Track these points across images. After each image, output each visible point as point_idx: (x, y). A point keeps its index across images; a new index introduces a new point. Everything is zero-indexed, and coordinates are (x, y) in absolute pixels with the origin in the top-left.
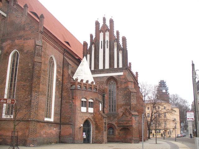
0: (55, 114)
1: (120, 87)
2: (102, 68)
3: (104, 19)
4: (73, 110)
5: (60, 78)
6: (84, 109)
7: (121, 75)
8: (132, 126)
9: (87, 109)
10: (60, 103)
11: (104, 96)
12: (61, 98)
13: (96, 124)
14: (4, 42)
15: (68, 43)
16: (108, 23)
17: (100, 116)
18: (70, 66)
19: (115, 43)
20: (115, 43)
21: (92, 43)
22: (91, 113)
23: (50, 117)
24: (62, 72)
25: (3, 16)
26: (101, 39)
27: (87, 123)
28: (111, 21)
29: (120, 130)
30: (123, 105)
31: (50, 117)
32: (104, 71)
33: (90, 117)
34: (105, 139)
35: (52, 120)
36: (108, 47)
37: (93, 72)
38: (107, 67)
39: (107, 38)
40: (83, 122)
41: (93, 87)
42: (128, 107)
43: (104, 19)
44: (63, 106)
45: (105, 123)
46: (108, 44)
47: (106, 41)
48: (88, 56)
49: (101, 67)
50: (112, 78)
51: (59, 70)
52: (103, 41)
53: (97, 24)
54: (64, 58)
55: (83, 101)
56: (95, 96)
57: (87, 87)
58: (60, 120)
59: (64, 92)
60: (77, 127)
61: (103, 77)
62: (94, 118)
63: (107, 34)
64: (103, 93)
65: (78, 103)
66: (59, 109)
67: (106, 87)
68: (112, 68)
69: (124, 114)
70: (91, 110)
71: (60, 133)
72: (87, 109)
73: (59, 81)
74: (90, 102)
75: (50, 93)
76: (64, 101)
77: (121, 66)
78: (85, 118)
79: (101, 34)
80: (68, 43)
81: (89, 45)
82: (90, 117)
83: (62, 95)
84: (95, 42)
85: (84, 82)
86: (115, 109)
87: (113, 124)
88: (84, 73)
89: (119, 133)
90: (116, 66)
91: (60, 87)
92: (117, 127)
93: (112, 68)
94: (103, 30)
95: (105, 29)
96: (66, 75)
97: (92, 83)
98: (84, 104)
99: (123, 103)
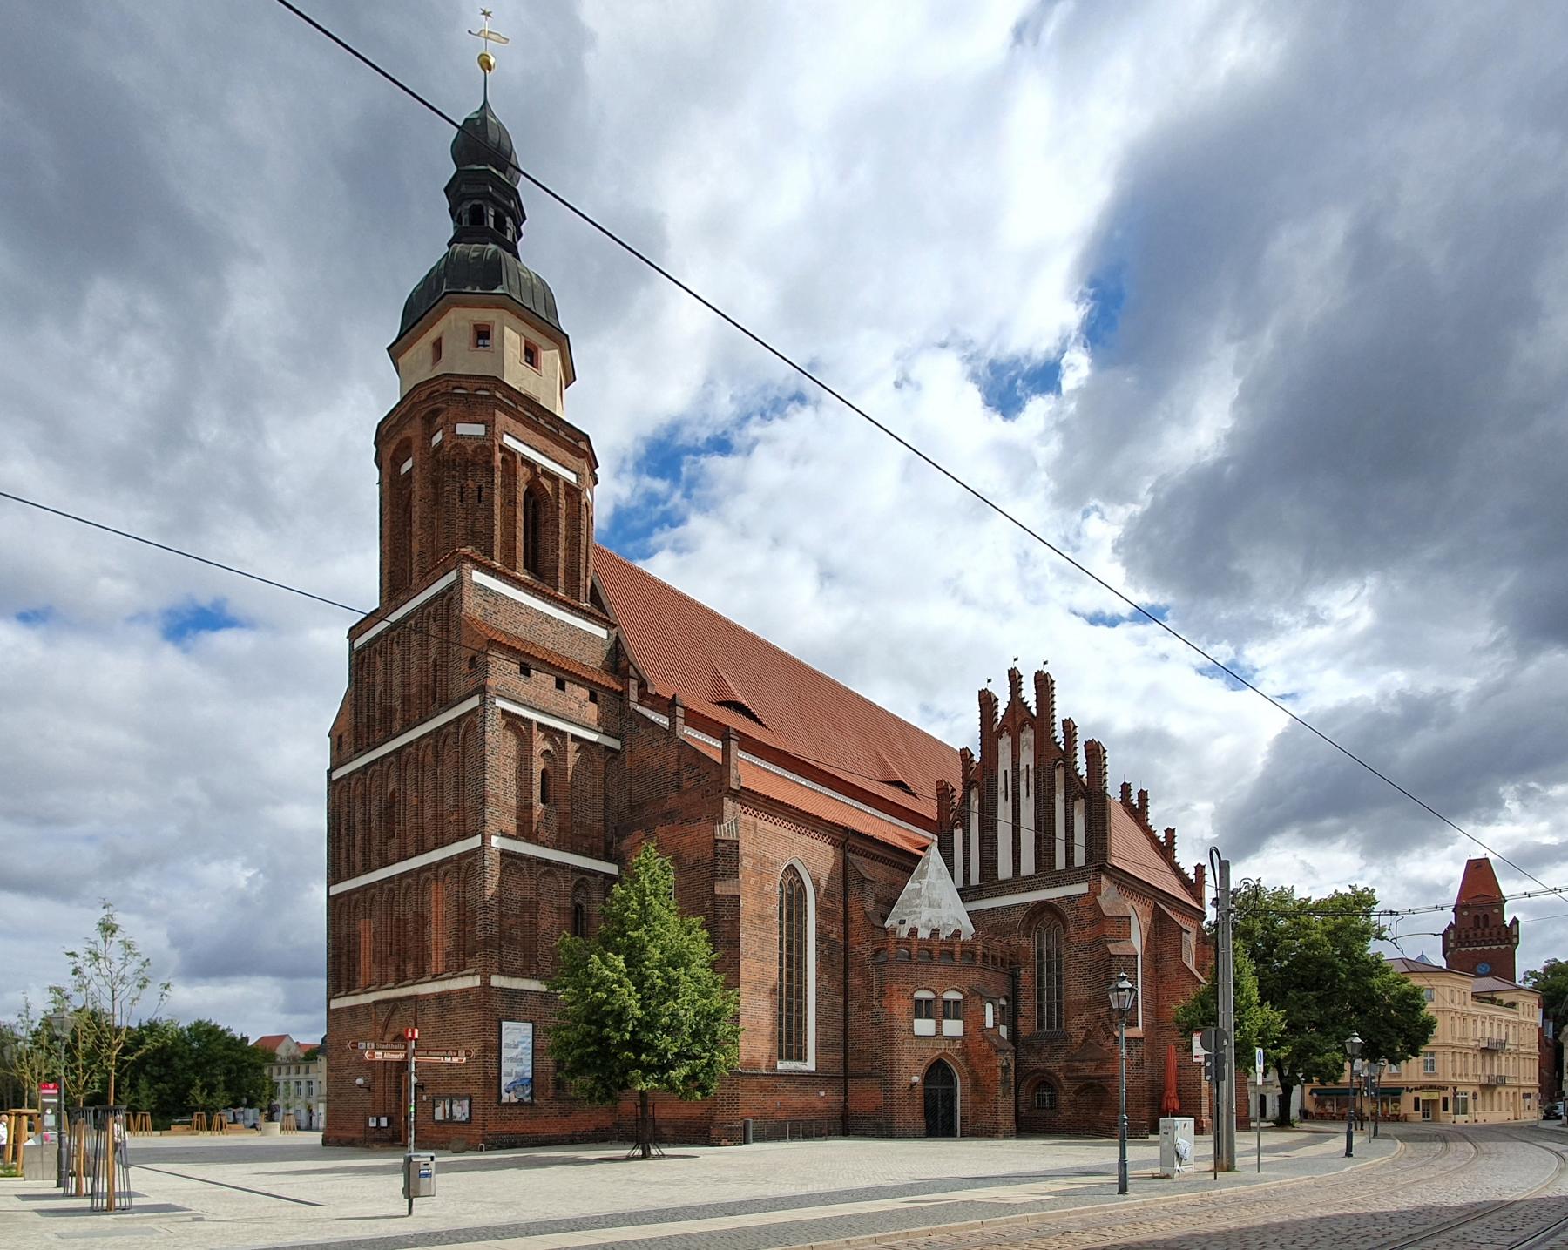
0: (821, 1045)
1: (1075, 941)
2: (1010, 875)
3: (1015, 678)
4: (885, 1032)
5: (835, 931)
6: (924, 1027)
7: (1079, 896)
8: (1113, 1077)
9: (939, 1026)
10: (840, 1010)
11: (1014, 977)
12: (846, 995)
13: (973, 1073)
14: (623, 837)
15: (900, 785)
16: (1029, 694)
17: (985, 1045)
18: (868, 887)
19: (1060, 775)
20: (1060, 775)
21: (968, 785)
22: (954, 1038)
23: (801, 1057)
24: (841, 910)
25: (607, 748)
26: (1005, 763)
27: (938, 1071)
28: (1044, 683)
29: (1077, 1093)
30: (1088, 1004)
31: (801, 1057)
32: (1018, 883)
33: (952, 1050)
34: (1006, 1119)
35: (810, 1065)
36: (1032, 791)
37: (966, 893)
38: (1028, 866)
39: (1027, 758)
40: (922, 1068)
41: (958, 950)
42: (1103, 1011)
43: (1015, 678)
44: (852, 1019)
45: (1006, 1069)
46: (1032, 780)
47: (1022, 768)
48: (958, 833)
49: (1005, 871)
50: (1045, 905)
51: (829, 905)
52: (1009, 769)
53: (987, 701)
54: (845, 860)
55: (919, 1001)
56: (974, 977)
57: (939, 952)
58: (846, 1066)
59: (851, 974)
60: (900, 1086)
61: (1014, 906)
62: (965, 1053)
63: (1028, 736)
64: (1010, 967)
65: (901, 1008)
66: (835, 1032)
67: (1024, 942)
68: (1046, 871)
69: (1088, 1034)
70: (953, 1027)
71: (845, 1107)
72: (939, 1026)
73: (832, 942)
74: (947, 1002)
75: (799, 982)
76: (854, 1005)
77: (1080, 859)
78: (931, 1056)
79: (1005, 744)
80: (900, 785)
81: (959, 793)
82: (952, 1050)
83: (846, 985)
84: (979, 774)
85: (924, 934)
86: (1060, 1019)
87: (1050, 1073)
88: (934, 903)
89: (1073, 1104)
90: (1060, 863)
91: (838, 958)
92: (1065, 1084)
93: (1046, 871)
94: (1010, 724)
95: (1019, 720)
96: (856, 916)
97: (957, 934)
98: (922, 1009)
99: (1086, 995)
